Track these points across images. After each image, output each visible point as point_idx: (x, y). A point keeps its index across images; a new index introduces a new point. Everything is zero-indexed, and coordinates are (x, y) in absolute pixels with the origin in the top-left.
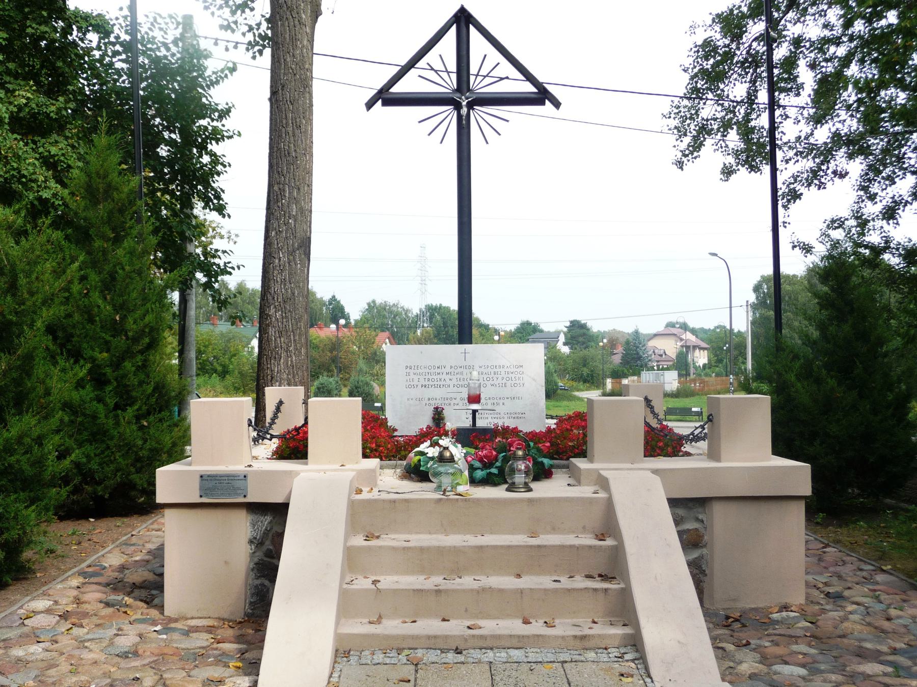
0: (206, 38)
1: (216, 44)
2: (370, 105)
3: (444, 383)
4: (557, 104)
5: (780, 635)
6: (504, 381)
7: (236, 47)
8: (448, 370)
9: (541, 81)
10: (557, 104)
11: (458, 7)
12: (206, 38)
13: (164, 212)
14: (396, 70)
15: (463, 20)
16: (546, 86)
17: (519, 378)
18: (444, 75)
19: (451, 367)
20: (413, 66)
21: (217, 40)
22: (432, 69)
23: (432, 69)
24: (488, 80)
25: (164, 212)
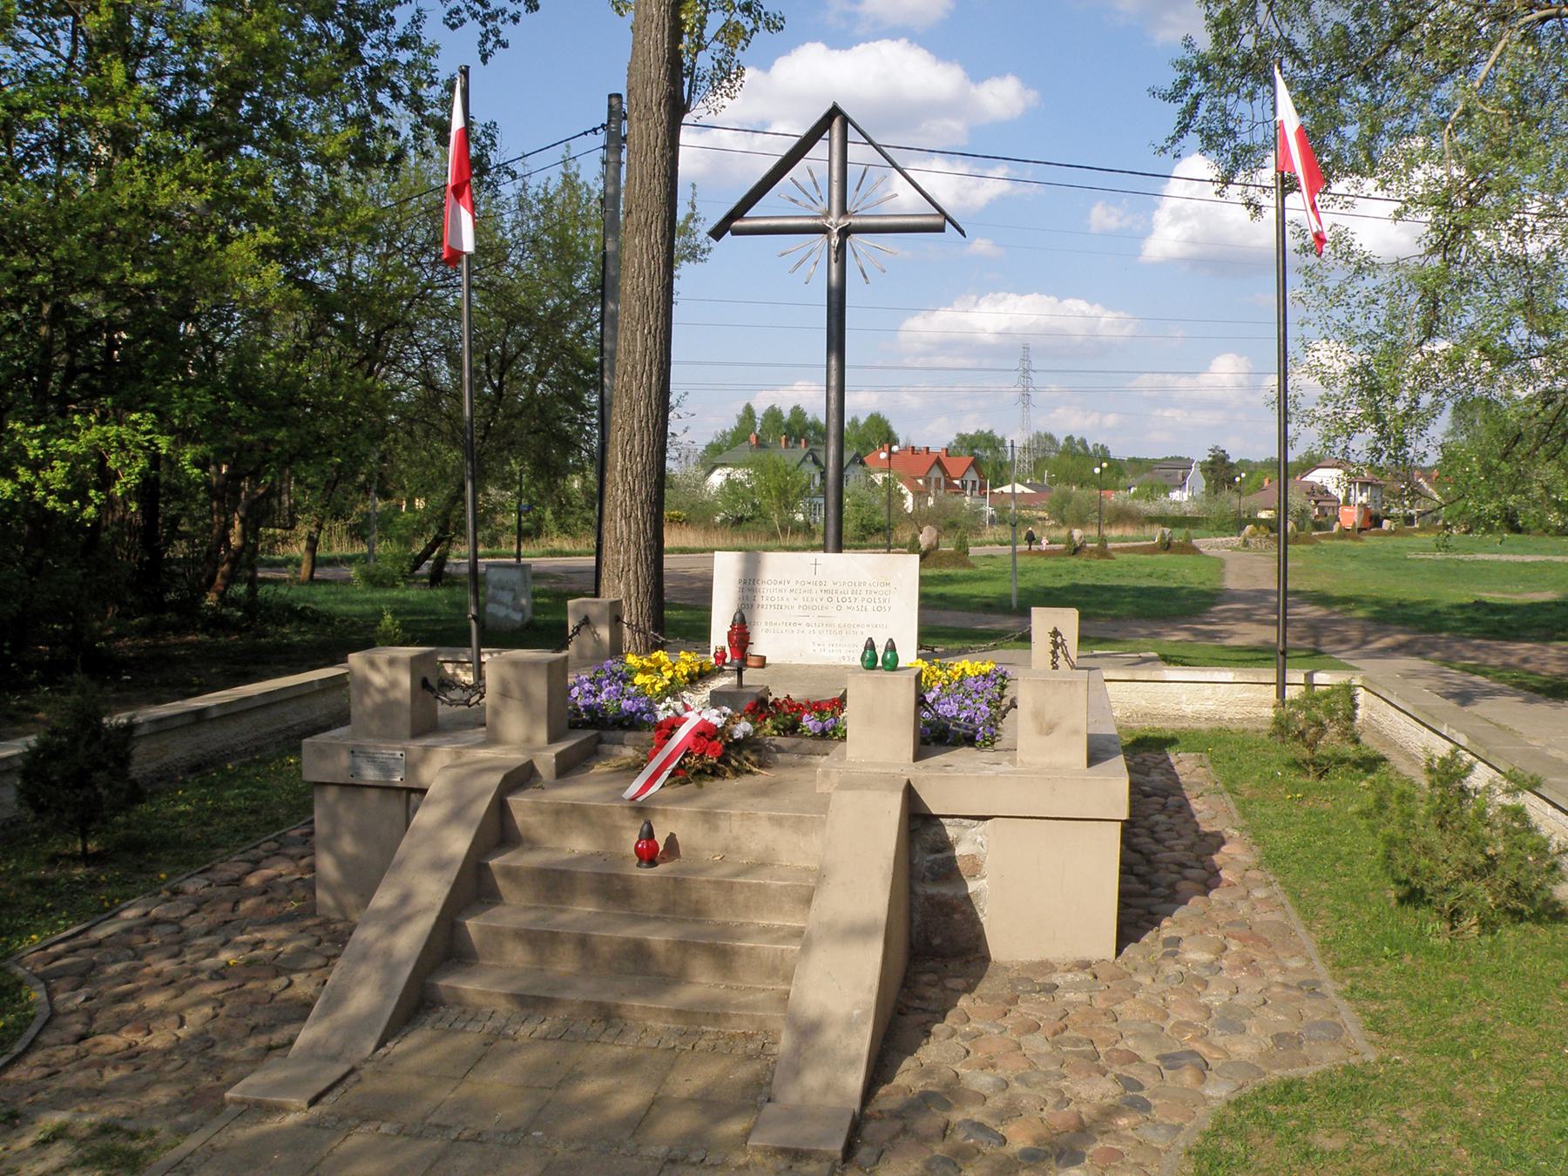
8: (792, 585)
11: (830, 106)
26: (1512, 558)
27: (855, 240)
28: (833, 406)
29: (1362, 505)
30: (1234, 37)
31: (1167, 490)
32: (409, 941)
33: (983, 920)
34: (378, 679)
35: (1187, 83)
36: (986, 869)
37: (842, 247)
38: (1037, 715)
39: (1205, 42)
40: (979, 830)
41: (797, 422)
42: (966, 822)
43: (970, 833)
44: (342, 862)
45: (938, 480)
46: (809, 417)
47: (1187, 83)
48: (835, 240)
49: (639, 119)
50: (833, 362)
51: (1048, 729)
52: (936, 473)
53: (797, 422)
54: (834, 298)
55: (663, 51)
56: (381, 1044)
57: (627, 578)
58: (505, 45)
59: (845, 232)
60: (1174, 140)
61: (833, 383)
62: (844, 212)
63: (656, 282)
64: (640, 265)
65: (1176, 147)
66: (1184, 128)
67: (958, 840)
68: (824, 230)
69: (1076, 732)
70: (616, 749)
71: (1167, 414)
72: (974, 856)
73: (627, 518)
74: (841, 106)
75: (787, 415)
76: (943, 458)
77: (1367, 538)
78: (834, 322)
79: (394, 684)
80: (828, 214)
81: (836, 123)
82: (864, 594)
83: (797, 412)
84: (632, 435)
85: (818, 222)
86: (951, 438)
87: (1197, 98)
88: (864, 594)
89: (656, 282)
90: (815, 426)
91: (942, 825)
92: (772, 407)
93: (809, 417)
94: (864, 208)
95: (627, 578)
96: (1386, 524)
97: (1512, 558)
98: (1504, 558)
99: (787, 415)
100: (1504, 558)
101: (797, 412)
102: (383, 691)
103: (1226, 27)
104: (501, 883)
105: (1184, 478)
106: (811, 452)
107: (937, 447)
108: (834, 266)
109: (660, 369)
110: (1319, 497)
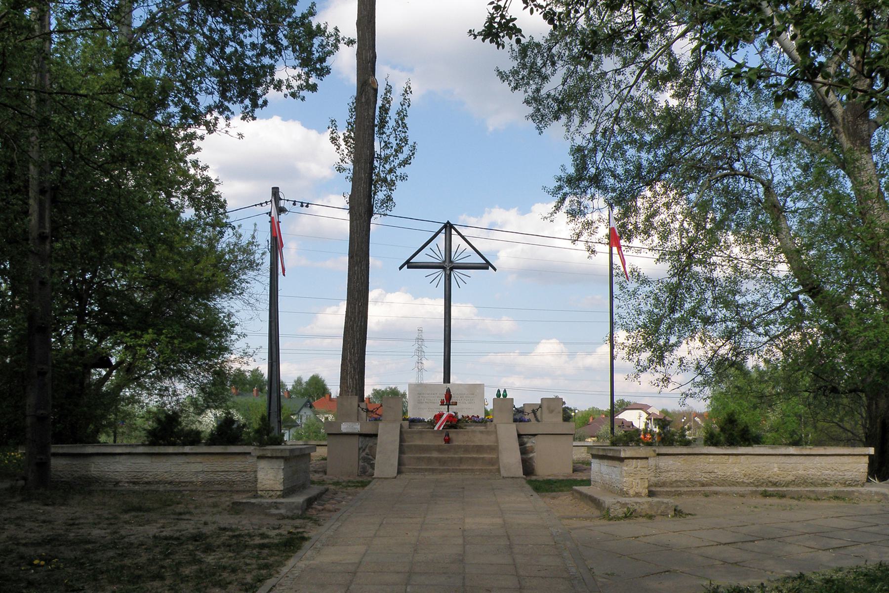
1: (294, 204)
7: (307, 206)
35: (560, 188)
39: (571, 170)
40: (533, 439)
48: (448, 272)
51: (551, 412)
59: (451, 269)
66: (558, 208)
80: (444, 262)
87: (565, 195)
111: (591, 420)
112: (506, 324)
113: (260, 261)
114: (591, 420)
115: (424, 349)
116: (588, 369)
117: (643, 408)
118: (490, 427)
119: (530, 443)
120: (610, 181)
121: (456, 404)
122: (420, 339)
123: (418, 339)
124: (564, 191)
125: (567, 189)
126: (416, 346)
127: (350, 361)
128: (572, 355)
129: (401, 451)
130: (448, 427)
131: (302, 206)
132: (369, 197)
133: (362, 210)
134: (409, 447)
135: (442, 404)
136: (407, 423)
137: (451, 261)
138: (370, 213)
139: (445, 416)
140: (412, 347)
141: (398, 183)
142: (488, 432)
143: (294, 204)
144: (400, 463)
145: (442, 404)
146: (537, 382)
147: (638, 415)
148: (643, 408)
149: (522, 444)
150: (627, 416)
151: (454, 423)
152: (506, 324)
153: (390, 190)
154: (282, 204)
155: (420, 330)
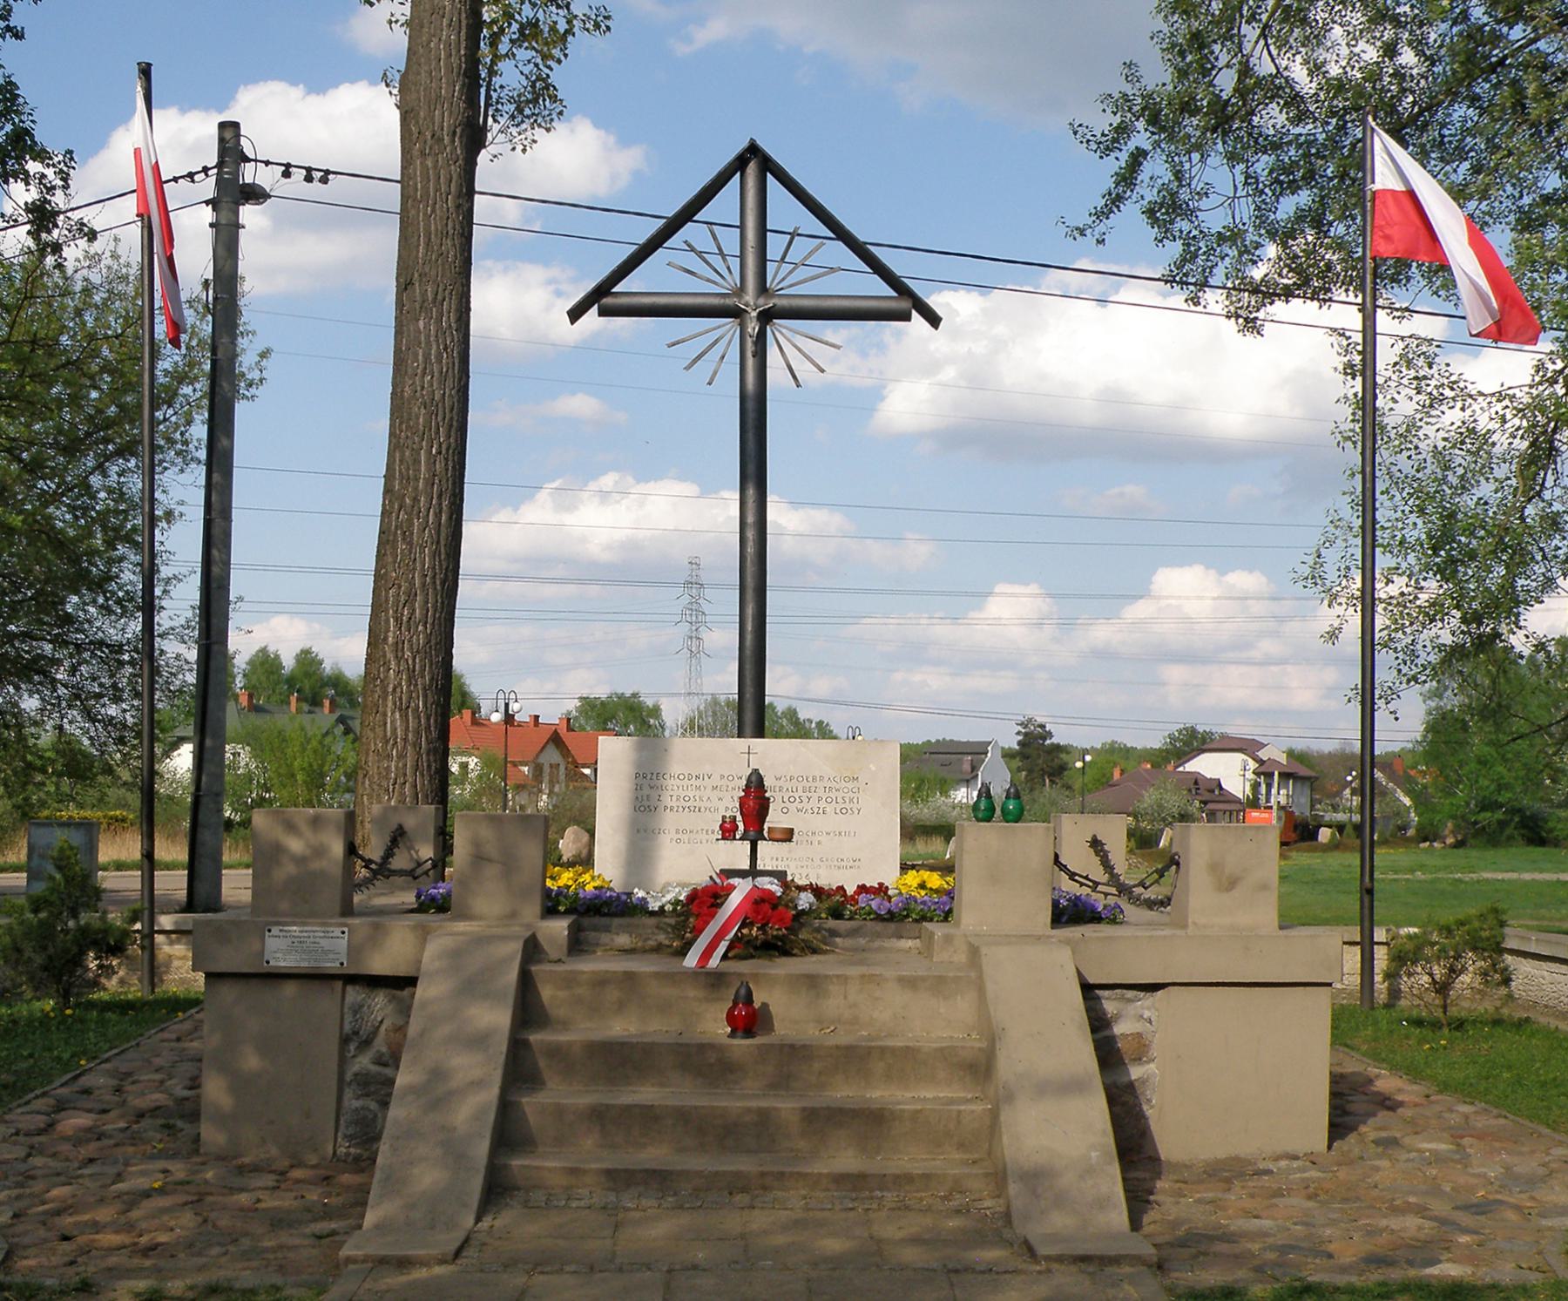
0: (267, 163)
1: (287, 174)
2: (575, 314)
3: (708, 805)
4: (934, 320)
5: (716, 342)
6: (823, 804)
7: (324, 180)
8: (716, 781)
9: (862, 239)
10: (934, 320)
11: (745, 144)
12: (267, 163)
13: (209, 1175)
14: (627, 252)
15: (754, 160)
16: (871, 248)
17: (851, 800)
18: (716, 261)
19: (722, 777)
20: (660, 245)
21: (288, 166)
22: (693, 249)
23: (693, 249)
24: (802, 273)
25: (209, 1175)
26: (1538, 876)
27: (782, 330)
28: (750, 549)
29: (1281, 808)
30: (1206, 69)
31: (945, 786)
32: (473, 1110)
33: (1149, 1112)
34: (295, 845)
35: (1122, 131)
36: (1154, 1052)
37: (762, 336)
38: (1215, 867)
39: (1158, 75)
40: (1146, 1005)
41: (307, 675)
42: (1130, 994)
43: (1132, 1009)
44: (240, 1084)
45: (554, 767)
46: (327, 667)
47: (1122, 131)
48: (753, 327)
49: (422, 154)
50: (751, 492)
51: (1229, 883)
52: (552, 756)
53: (307, 675)
54: (750, 405)
55: (458, 60)
56: (478, 1219)
57: (402, 794)
58: (19, 35)
59: (767, 317)
60: (1102, 214)
61: (750, 519)
62: (763, 289)
63: (449, 383)
64: (427, 357)
65: (1102, 228)
66: (1115, 202)
67: (1118, 1017)
68: (736, 313)
69: (1265, 887)
70: (605, 938)
71: (917, 678)
72: (1139, 1035)
73: (404, 712)
74: (761, 143)
75: (288, 662)
76: (563, 732)
77: (1294, 854)
78: (751, 436)
79: (320, 852)
80: (741, 290)
81: (752, 169)
82: (821, 792)
83: (307, 660)
84: (411, 596)
85: (728, 301)
86: (572, 705)
87: (1138, 157)
88: (821, 792)
89: (449, 383)
90: (337, 682)
91: (1099, 998)
92: (264, 650)
93: (327, 667)
94: (790, 283)
95: (402, 794)
96: (1325, 834)
97: (1538, 876)
98: (1527, 876)
99: (288, 662)
100: (1527, 876)
101: (307, 660)
102: (301, 861)
103: (1192, 52)
104: (542, 1063)
105: (974, 768)
106: (342, 720)
107: (552, 715)
108: (750, 362)
109: (452, 504)
110: (1207, 796)
111: (1117, 775)
112: (918, 552)
113: (255, 375)
114: (1117, 775)
115: (705, 607)
116: (1103, 655)
117: (1247, 747)
118: (946, 946)
119: (1110, 1005)
120: (1273, 118)
121: (788, 835)
122: (694, 584)
123: (688, 584)
124: (1132, 145)
125: (1142, 138)
126: (686, 599)
127: (398, 647)
128: (1067, 624)
129: (520, 1069)
130: (743, 948)
131: (309, 179)
132: (472, 78)
133: (447, 119)
134: (556, 1053)
135: (728, 831)
136: (559, 928)
137: (763, 289)
138: (475, 139)
139: (735, 899)
140: (674, 601)
141: (580, 43)
142: (941, 980)
143: (287, 174)
144: (509, 1134)
145: (728, 831)
146: (979, 681)
147: (1239, 766)
148: (1247, 747)
149: (1099, 1024)
150: (1206, 765)
151: (775, 930)
152: (918, 552)
153: (546, 57)
154: (249, 174)
155: (694, 563)
